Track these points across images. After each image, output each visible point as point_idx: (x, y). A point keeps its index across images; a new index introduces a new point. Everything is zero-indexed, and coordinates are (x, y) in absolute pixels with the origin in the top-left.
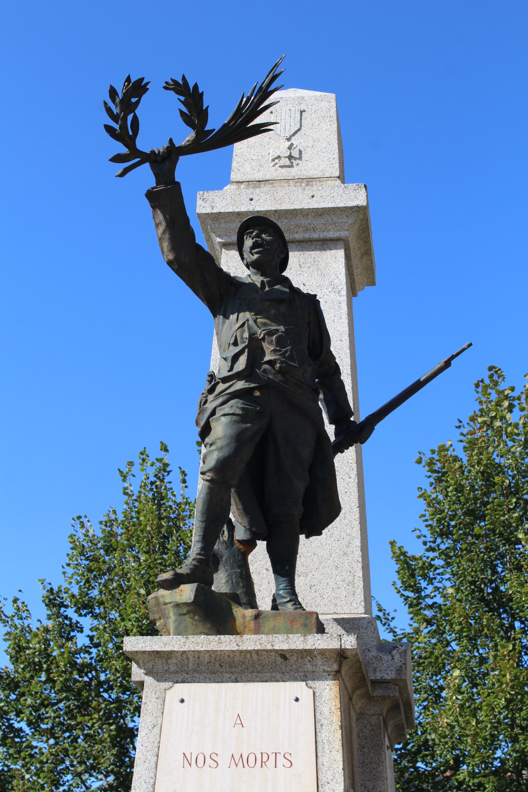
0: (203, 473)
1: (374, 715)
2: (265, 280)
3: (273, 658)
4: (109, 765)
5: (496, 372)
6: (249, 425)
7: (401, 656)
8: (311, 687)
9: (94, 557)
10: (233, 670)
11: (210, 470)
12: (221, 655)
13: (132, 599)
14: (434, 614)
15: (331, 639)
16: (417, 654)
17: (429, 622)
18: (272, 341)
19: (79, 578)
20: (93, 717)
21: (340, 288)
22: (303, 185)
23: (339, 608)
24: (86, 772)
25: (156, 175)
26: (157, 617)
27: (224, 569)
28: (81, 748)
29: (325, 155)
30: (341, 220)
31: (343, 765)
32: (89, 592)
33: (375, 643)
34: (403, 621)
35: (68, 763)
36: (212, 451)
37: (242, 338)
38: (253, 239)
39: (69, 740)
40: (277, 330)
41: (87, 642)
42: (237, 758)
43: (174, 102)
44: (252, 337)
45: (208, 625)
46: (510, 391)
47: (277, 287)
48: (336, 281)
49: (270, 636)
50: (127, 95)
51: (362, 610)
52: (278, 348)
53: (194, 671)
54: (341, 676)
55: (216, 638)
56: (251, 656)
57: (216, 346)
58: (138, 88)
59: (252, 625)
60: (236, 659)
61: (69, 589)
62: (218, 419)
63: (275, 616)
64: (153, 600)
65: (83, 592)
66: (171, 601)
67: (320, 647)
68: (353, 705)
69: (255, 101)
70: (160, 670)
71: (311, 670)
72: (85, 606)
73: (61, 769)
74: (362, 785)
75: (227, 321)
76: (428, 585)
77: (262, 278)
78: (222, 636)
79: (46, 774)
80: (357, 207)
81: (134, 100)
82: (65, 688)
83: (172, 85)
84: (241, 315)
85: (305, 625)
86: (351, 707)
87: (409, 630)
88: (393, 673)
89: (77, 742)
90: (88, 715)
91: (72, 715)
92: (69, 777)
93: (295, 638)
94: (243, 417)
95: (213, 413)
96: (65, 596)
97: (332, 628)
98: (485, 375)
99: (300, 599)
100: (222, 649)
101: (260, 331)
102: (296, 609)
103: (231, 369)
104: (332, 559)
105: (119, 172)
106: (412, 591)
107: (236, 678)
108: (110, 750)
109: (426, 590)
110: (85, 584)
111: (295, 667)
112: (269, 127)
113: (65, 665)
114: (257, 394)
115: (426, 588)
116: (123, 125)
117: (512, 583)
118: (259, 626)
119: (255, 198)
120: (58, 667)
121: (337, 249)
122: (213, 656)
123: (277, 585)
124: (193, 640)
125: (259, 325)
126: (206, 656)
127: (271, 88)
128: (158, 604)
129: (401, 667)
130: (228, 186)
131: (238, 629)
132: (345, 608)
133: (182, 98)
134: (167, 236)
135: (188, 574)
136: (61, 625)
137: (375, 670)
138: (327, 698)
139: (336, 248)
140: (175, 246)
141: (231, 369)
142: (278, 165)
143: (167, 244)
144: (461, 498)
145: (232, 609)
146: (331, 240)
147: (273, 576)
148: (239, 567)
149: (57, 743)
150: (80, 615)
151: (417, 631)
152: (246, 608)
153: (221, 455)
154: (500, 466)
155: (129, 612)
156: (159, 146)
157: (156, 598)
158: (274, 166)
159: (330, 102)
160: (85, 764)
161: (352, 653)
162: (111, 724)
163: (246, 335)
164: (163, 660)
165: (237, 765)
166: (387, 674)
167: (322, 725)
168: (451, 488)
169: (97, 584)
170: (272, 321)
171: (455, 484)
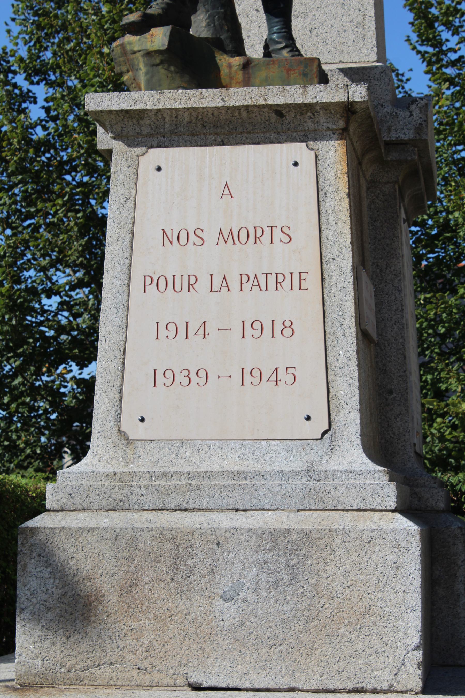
1: (388, 182)
3: (267, 115)
4: (78, 258)
7: (421, 112)
8: (312, 149)
9: (44, 11)
10: (219, 130)
12: (203, 113)
13: (93, 60)
14: (458, 72)
15: (337, 90)
16: (437, 119)
17: (451, 81)
19: (27, 37)
20: (56, 202)
23: (346, 56)
24: (51, 267)
26: (124, 69)
27: (204, 9)
28: (43, 239)
31: (352, 238)
32: (41, 54)
33: (389, 97)
34: (419, 83)
35: (29, 256)
39: (29, 230)
41: (43, 115)
42: (226, 234)
45: (187, 78)
49: (262, 89)
51: (374, 57)
53: (172, 133)
54: (349, 134)
55: (191, 92)
56: (240, 113)
59: (240, 76)
60: (221, 117)
61: (16, 52)
63: (268, 64)
65: (33, 54)
66: (140, 49)
67: (323, 100)
68: (363, 171)
70: (131, 134)
72: (37, 72)
73: (22, 264)
74: (373, 263)
76: (453, 35)
78: (204, 90)
79: (4, 269)
82: (21, 170)
85: (305, 75)
86: (361, 174)
87: (427, 91)
88: (411, 132)
89: (38, 232)
90: (50, 201)
91: (31, 201)
92: (32, 273)
96: (11, 59)
97: (338, 80)
99: (298, 45)
100: (205, 106)
102: (293, 56)
106: (431, 46)
107: (222, 141)
108: (77, 240)
109: (448, 43)
110: (35, 45)
111: (292, 125)
113: (19, 142)
115: (447, 40)
118: (249, 78)
120: (11, 144)
122: (194, 114)
123: (270, 28)
124: (170, 95)
126: (186, 115)
128: (124, 52)
129: (421, 124)
131: (223, 81)
132: (353, 55)
135: (159, 14)
136: (9, 93)
137: (389, 130)
138: (332, 161)
145: (215, 57)
147: (264, 16)
148: (223, 6)
149: (14, 235)
150: (32, 83)
151: (439, 94)
152: (232, 57)
155: (91, 76)
157: (122, 46)
160: (50, 256)
161: (362, 107)
162: (78, 211)
164: (134, 121)
165: (226, 242)
166: (404, 134)
167: (326, 193)
169: (50, 44)
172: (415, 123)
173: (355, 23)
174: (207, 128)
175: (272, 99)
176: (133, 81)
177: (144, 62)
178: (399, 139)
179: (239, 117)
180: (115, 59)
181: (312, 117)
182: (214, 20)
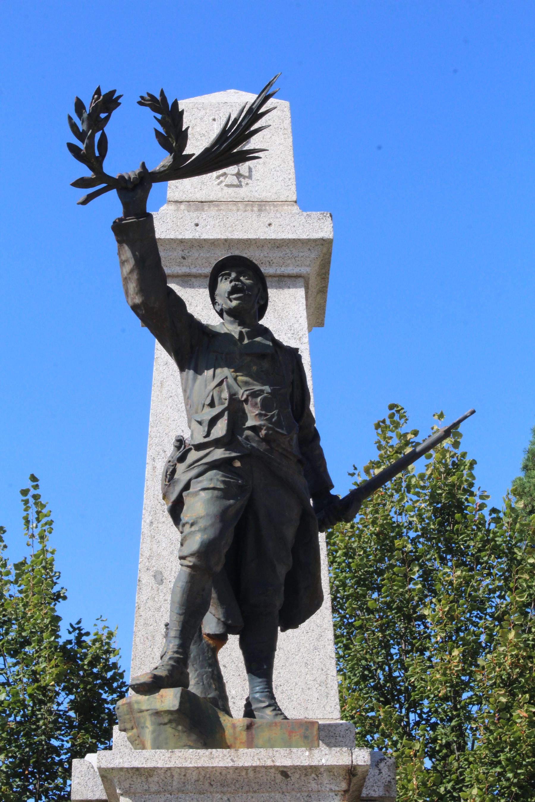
0: (181, 558)
2: (244, 330)
3: (273, 775)
5: (398, 411)
6: (232, 502)
7: (389, 770)
10: (225, 789)
11: (192, 555)
12: (212, 772)
15: (341, 754)
18: (256, 404)
21: (301, 334)
22: (256, 209)
25: (125, 205)
29: (279, 174)
30: (302, 254)
36: (194, 532)
37: (220, 398)
38: (231, 282)
40: (262, 391)
43: (150, 121)
44: (233, 397)
45: (194, 737)
46: (413, 436)
47: (258, 339)
48: (296, 326)
50: (96, 111)
52: (263, 412)
55: (201, 752)
56: (247, 773)
57: (172, 404)
58: (108, 102)
59: (244, 736)
60: (228, 776)
62: (196, 494)
64: (125, 707)
66: (148, 708)
67: (329, 763)
69: (243, 124)
70: (139, 790)
71: (316, 790)
75: (199, 377)
77: (239, 328)
78: (214, 750)
80: (323, 240)
81: (103, 116)
83: (148, 101)
84: (218, 371)
85: (306, 737)
88: (381, 789)
93: (300, 753)
94: (226, 492)
95: (187, 487)
98: (385, 414)
99: (279, 704)
100: (214, 765)
101: (241, 391)
102: (277, 715)
103: (208, 435)
104: (300, 654)
105: (82, 199)
111: (297, 786)
112: (256, 155)
114: (238, 464)
116: (90, 151)
117: (415, 669)
118: (252, 738)
119: (202, 223)
121: (296, 287)
123: (252, 687)
124: (180, 754)
125: (240, 384)
126: (194, 773)
127: (262, 110)
129: (390, 782)
130: (165, 207)
131: (228, 741)
132: (317, 712)
133: (159, 116)
134: (135, 276)
139: (295, 286)
140: (143, 288)
141: (208, 435)
142: (224, 184)
143: (134, 285)
144: (352, 565)
145: (219, 718)
146: (290, 276)
148: (210, 665)
153: (205, 537)
154: (398, 526)
156: (131, 171)
158: (218, 184)
159: (283, 111)
163: (225, 395)
166: (374, 791)
168: (340, 552)
170: (255, 380)
171: (346, 547)
172: (384, 781)
173: (318, 682)
174: (214, 787)
175: (279, 760)
176: (137, 738)
177: (151, 720)
178: (369, 795)
179: (245, 777)
180: (120, 716)
181: (316, 778)
182: (202, 679)
